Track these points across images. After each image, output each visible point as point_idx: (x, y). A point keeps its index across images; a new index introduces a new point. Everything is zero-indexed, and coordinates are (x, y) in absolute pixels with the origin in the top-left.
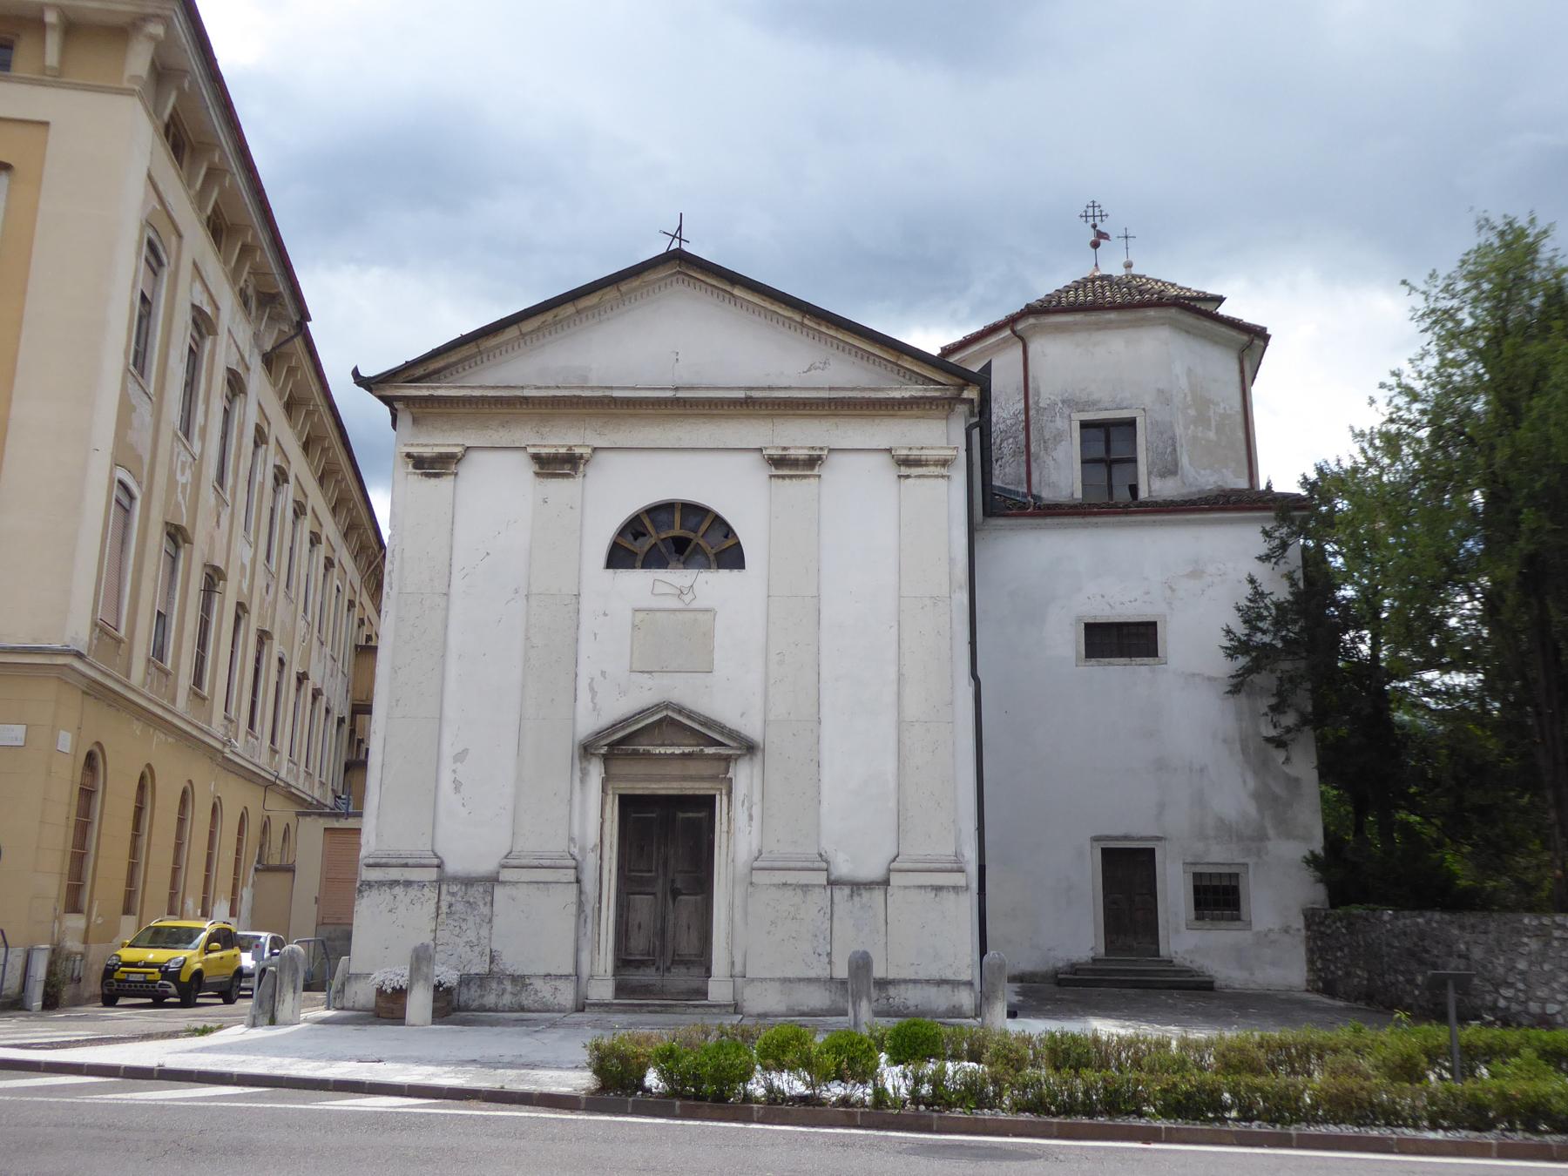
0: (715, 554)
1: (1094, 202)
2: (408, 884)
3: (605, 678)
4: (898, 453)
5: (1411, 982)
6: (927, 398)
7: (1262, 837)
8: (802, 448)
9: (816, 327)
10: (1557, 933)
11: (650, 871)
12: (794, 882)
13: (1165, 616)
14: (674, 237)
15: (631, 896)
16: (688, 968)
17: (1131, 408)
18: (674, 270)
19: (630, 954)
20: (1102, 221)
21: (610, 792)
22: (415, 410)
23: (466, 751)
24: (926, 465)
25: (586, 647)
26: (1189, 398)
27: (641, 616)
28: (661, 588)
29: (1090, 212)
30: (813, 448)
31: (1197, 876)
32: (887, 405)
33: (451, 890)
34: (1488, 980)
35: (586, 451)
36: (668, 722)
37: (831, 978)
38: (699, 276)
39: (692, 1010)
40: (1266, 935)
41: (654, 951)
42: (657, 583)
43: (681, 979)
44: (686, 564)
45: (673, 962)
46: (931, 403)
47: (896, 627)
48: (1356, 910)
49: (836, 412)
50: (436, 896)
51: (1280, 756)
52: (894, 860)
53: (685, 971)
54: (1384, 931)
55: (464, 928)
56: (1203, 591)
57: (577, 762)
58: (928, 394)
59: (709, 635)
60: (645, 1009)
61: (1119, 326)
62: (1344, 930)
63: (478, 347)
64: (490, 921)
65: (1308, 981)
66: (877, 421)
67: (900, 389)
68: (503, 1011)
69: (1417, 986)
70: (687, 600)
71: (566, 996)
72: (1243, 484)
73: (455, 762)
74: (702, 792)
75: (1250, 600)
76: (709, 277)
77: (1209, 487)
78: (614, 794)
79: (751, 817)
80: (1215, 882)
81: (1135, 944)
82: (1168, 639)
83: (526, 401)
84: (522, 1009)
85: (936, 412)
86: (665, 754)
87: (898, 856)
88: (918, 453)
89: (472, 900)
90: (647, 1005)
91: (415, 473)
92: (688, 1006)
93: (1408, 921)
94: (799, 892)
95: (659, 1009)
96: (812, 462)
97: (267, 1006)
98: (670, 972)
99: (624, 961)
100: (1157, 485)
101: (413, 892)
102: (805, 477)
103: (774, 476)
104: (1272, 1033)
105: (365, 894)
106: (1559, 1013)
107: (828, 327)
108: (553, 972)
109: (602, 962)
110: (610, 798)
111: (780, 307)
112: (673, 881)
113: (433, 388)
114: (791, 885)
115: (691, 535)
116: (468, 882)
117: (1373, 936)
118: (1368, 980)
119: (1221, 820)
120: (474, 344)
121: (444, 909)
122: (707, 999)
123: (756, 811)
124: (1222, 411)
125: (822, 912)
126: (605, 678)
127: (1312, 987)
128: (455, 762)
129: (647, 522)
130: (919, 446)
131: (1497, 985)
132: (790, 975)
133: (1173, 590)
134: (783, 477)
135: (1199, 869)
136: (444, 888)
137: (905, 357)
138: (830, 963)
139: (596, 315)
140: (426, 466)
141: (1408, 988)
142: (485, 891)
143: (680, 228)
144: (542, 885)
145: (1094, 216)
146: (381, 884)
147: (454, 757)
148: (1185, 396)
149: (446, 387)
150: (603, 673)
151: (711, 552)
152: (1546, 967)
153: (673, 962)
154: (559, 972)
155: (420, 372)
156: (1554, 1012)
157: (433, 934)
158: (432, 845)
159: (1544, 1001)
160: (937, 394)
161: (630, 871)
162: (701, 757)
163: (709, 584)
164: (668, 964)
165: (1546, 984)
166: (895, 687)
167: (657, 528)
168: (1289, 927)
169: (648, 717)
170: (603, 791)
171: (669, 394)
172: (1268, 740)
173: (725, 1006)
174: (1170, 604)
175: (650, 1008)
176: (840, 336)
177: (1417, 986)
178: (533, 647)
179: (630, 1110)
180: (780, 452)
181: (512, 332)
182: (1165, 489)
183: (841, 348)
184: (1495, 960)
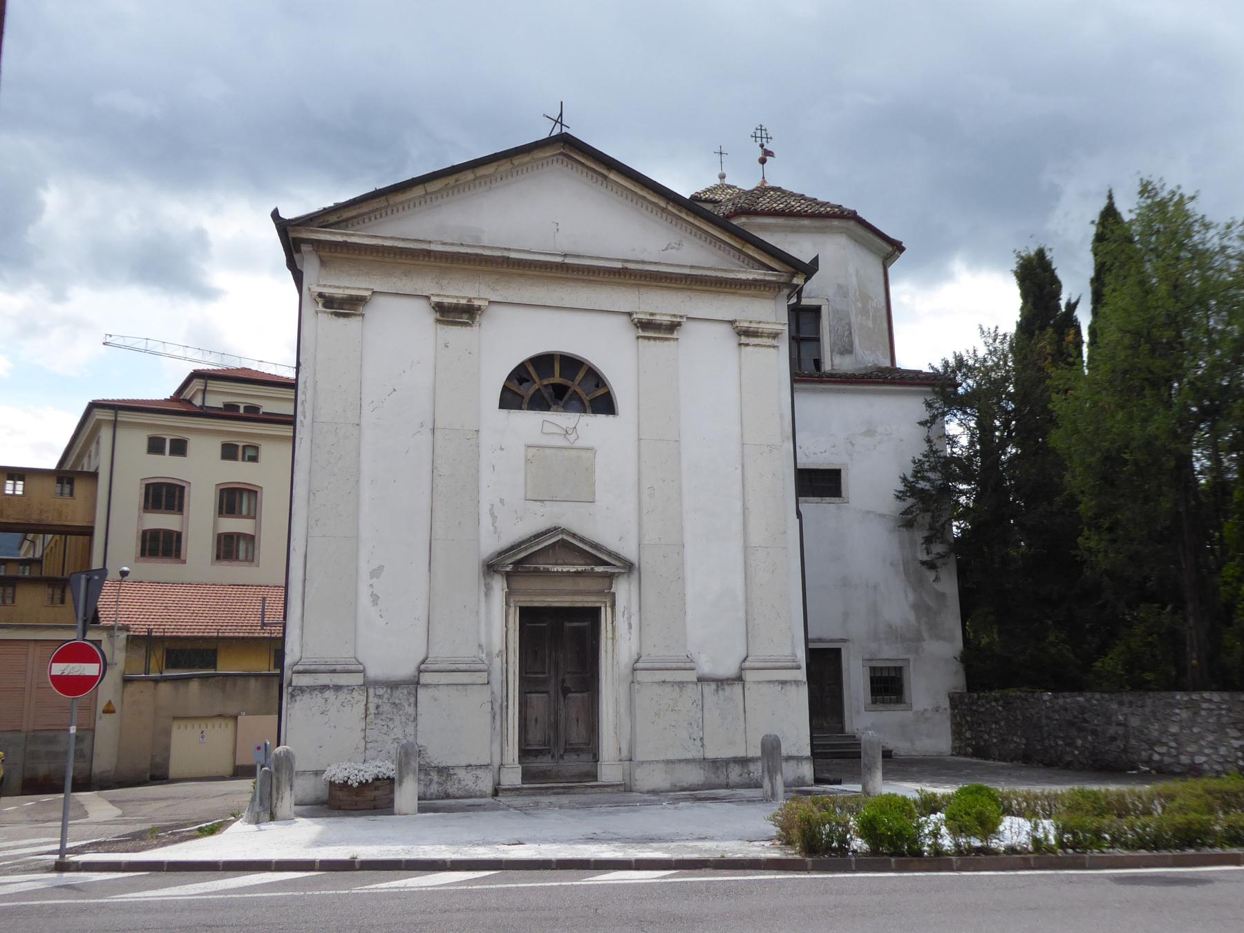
0: (590, 401)
1: (761, 126)
2: (338, 688)
3: (503, 505)
4: (741, 325)
5: (1071, 744)
6: (765, 281)
7: (919, 639)
8: (666, 315)
9: (677, 213)
10: (1205, 705)
11: (545, 673)
12: (671, 680)
13: (847, 465)
14: (557, 121)
15: (529, 695)
16: (578, 755)
17: (818, 298)
18: (559, 151)
19: (528, 745)
20: (767, 142)
21: (512, 605)
22: (323, 254)
23: (381, 568)
24: (761, 336)
25: (486, 478)
26: (857, 293)
27: (532, 451)
28: (549, 428)
29: (759, 134)
30: (674, 315)
31: (873, 669)
32: (635, 276)
33: (377, 693)
34: (1144, 742)
35: (483, 303)
36: (563, 544)
37: (704, 759)
38: (583, 160)
39: (589, 790)
40: (922, 714)
41: (549, 742)
42: (545, 424)
43: (573, 764)
44: (566, 408)
45: (566, 751)
46: (765, 286)
47: (740, 468)
48: (1013, 693)
49: (690, 287)
50: (365, 699)
51: (931, 575)
52: (744, 660)
53: (576, 757)
54: (1044, 708)
55: (392, 726)
56: (875, 446)
57: (482, 579)
58: (767, 278)
59: (590, 470)
60: (551, 791)
61: (809, 230)
62: (1000, 708)
63: (387, 201)
64: (415, 719)
65: (954, 748)
66: (722, 297)
67: (745, 272)
68: (431, 799)
69: (1076, 748)
70: (572, 440)
71: (486, 785)
72: (888, 364)
73: (372, 578)
74: (590, 605)
75: (925, 456)
76: (588, 161)
77: (870, 365)
78: (515, 607)
79: (630, 626)
80: (885, 674)
81: (825, 724)
82: (850, 483)
83: (428, 254)
84: (448, 796)
85: (767, 293)
86: (562, 572)
87: (427, 658)
88: (757, 326)
89: (397, 701)
90: (552, 788)
91: (325, 312)
92: (587, 787)
93: (1068, 700)
94: (676, 688)
95: (561, 790)
96: (673, 327)
97: (267, 805)
98: (563, 759)
99: (525, 752)
100: (838, 360)
101: (343, 695)
102: (667, 339)
103: (642, 337)
104: (998, 787)
105: (298, 698)
106: (1205, 762)
107: (687, 215)
108: (472, 763)
109: (510, 753)
110: (512, 610)
111: (649, 193)
112: (563, 681)
113: (347, 235)
114: (668, 682)
115: (569, 383)
116: (393, 685)
117: (1033, 712)
118: (1025, 744)
119: (890, 626)
120: (383, 198)
121: (372, 710)
122: (597, 781)
123: (635, 621)
124: (875, 305)
125: (695, 704)
126: (503, 505)
127: (957, 751)
128: (372, 578)
129: (531, 370)
130: (758, 320)
131: (1152, 744)
132: (672, 758)
133: (853, 445)
134: (649, 338)
135: (874, 664)
136: (371, 691)
137: (749, 246)
138: (703, 746)
139: (488, 183)
140: (335, 306)
141: (1068, 749)
142: (409, 693)
143: (561, 115)
144: (460, 687)
145: (762, 138)
146: (312, 689)
147: (371, 573)
148: (856, 292)
149: (359, 235)
150: (502, 501)
151: (586, 399)
152: (1195, 730)
153: (566, 751)
154: (479, 763)
155: (333, 219)
156: (1201, 762)
157: (363, 734)
158: (355, 654)
159: (1192, 755)
160: (774, 279)
161: (526, 673)
162: (592, 574)
163: (590, 426)
164: (562, 752)
165: (1195, 742)
166: (741, 517)
167: (541, 377)
168: (939, 707)
169: (546, 540)
170: (506, 604)
171: (559, 259)
172: (923, 563)
173: (618, 785)
174: (850, 455)
175: (555, 791)
176: (697, 223)
177: (1076, 748)
178: (440, 475)
179: (854, 868)
180: (649, 317)
181: (418, 191)
182: (845, 364)
183: (693, 233)
184: (1150, 726)
